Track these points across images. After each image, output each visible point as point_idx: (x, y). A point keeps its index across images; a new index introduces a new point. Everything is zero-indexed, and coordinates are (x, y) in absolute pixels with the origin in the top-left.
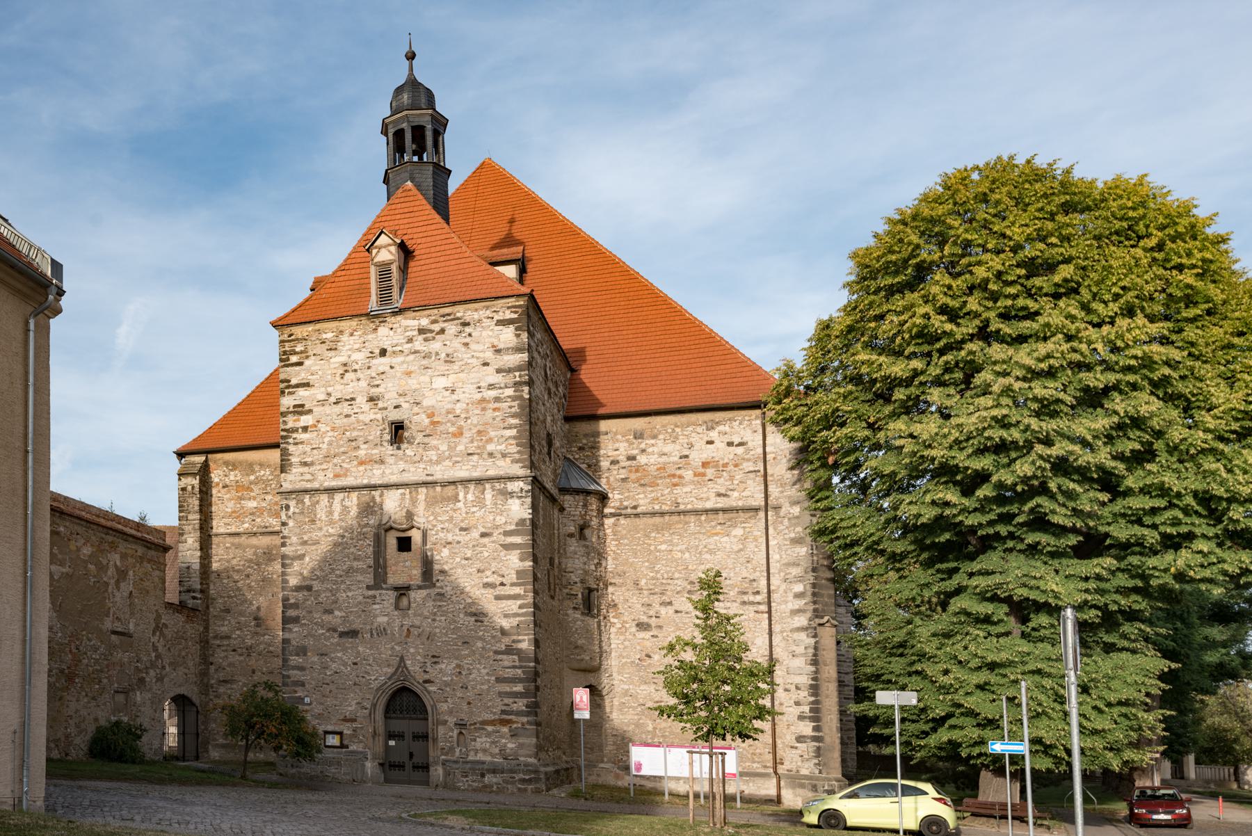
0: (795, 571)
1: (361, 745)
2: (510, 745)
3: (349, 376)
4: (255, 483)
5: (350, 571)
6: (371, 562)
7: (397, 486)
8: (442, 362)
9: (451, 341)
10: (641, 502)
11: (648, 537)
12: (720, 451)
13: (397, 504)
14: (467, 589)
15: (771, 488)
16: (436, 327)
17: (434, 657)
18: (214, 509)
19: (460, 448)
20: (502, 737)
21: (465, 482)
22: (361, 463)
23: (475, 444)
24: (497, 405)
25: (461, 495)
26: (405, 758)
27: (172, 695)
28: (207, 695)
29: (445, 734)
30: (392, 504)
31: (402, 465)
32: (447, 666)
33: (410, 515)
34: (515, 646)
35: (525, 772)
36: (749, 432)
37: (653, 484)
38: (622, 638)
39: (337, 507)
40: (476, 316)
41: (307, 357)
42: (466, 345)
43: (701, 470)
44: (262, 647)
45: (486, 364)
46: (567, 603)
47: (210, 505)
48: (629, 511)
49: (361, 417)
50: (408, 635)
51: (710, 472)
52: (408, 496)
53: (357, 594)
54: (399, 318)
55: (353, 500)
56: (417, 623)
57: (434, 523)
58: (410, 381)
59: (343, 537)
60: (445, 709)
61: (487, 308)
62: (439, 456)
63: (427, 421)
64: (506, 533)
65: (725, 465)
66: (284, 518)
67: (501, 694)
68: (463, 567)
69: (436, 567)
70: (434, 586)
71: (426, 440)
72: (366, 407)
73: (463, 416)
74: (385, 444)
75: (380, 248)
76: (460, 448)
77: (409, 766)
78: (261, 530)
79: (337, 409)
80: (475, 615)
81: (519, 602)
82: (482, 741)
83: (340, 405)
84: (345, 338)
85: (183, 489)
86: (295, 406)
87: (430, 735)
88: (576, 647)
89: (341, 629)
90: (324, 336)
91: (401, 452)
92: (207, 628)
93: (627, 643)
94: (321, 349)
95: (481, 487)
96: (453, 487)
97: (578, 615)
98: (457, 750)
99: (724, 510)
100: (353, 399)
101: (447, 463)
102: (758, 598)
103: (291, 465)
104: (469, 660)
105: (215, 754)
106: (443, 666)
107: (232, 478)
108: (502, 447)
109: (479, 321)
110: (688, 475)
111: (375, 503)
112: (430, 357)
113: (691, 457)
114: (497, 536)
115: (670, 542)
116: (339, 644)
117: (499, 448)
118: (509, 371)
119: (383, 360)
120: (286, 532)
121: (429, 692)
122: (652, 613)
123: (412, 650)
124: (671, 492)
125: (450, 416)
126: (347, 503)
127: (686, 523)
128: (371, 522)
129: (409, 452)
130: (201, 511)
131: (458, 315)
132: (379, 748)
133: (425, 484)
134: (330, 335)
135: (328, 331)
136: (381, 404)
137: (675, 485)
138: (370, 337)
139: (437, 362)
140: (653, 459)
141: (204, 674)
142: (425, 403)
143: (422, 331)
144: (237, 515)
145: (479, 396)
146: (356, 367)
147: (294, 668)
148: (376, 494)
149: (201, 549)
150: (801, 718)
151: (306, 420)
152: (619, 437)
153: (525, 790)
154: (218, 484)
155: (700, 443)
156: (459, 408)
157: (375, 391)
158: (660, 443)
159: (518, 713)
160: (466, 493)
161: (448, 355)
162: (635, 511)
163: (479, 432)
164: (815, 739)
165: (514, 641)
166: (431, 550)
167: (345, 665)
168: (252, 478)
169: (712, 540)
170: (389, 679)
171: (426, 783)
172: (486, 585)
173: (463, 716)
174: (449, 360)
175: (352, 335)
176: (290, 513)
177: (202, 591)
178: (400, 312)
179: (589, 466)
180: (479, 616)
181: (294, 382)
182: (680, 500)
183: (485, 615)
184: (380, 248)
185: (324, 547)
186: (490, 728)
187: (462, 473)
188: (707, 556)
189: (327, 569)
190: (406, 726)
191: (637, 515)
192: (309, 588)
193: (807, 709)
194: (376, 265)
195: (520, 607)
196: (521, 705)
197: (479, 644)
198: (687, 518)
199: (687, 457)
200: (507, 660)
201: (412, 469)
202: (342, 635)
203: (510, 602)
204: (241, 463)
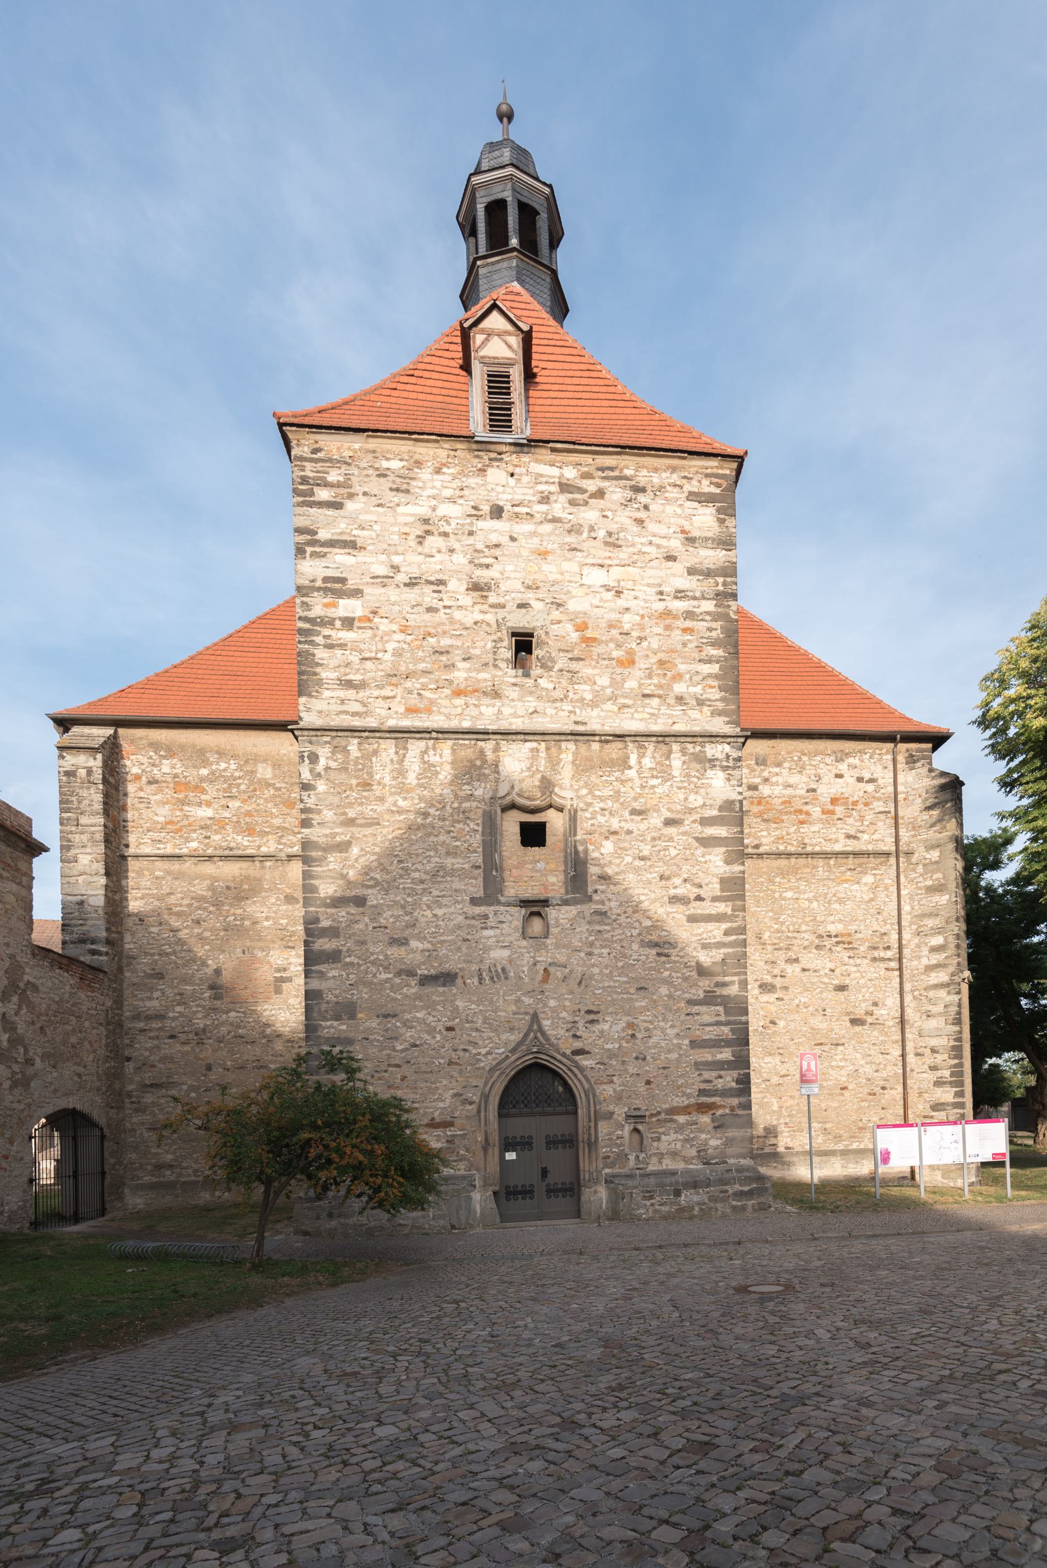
1: (462, 1165)
2: (714, 1143)
3: (433, 542)
4: (213, 778)
5: (437, 874)
7: (526, 735)
8: (598, 543)
9: (611, 510)
10: (764, 841)
11: (771, 881)
12: (848, 786)
13: (523, 766)
14: (645, 905)
15: (902, 832)
16: (591, 486)
17: (589, 1012)
18: (130, 816)
19: (631, 684)
20: (702, 1131)
21: (640, 737)
22: (458, 693)
23: (655, 681)
24: (688, 624)
25: (633, 759)
27: (50, 1110)
28: (120, 1108)
29: (612, 1134)
30: (516, 764)
31: (532, 703)
32: (612, 1027)
33: (547, 785)
34: (719, 991)
36: (880, 767)
37: (778, 821)
40: (656, 480)
41: (351, 496)
42: (640, 522)
44: (224, 1029)
45: (671, 558)
47: (124, 808)
49: (458, 615)
51: (839, 810)
52: (543, 755)
54: (525, 458)
55: (444, 753)
56: (562, 959)
57: (589, 799)
58: (545, 567)
59: (426, 815)
60: (609, 1094)
61: (674, 469)
62: (596, 694)
64: (705, 822)
66: (306, 775)
67: (698, 1066)
68: (637, 871)
69: (593, 870)
70: (590, 899)
71: (574, 666)
72: (467, 600)
73: (635, 634)
74: (503, 665)
75: (489, 334)
76: (631, 684)
78: (219, 852)
79: (412, 595)
80: (657, 945)
81: (725, 926)
82: (670, 1140)
83: (416, 590)
84: (425, 474)
85: (68, 774)
86: (325, 579)
87: (582, 1135)
89: (422, 971)
90: (385, 464)
91: (529, 682)
92: (119, 1003)
94: (375, 485)
96: (619, 745)
98: (632, 1157)
99: (856, 854)
100: (441, 582)
101: (609, 706)
102: (889, 954)
103: (320, 683)
104: (648, 1016)
105: (136, 1201)
106: (606, 1027)
107: (166, 769)
108: (698, 689)
109: (661, 488)
110: (816, 811)
111: (485, 761)
112: (579, 532)
113: (819, 791)
114: (689, 824)
117: (692, 689)
118: (708, 573)
119: (496, 524)
120: (311, 802)
121: (582, 1069)
122: (776, 971)
123: (552, 1003)
124: (798, 831)
125: (614, 632)
126: (432, 758)
127: (814, 867)
128: (479, 793)
129: (543, 683)
130: (106, 813)
131: (628, 472)
132: (494, 1167)
134: (395, 464)
135: (395, 454)
136: (493, 599)
137: (802, 822)
138: (473, 481)
139: (592, 543)
140: (777, 790)
141: (115, 1075)
142: (573, 605)
143: (565, 487)
144: (177, 828)
145: (660, 606)
146: (447, 529)
148: (488, 746)
149: (107, 874)
151: (347, 607)
153: (743, 1208)
154: (138, 777)
155: (828, 778)
156: (628, 621)
157: (482, 575)
158: (785, 772)
159: (725, 1093)
160: (641, 756)
161: (610, 534)
163: (661, 663)
165: (717, 985)
166: (584, 842)
167: (431, 1031)
168: (204, 772)
169: (840, 888)
170: (513, 1051)
172: (674, 900)
173: (638, 1103)
174: (613, 542)
175: (438, 471)
176: (320, 768)
177: (108, 942)
178: (531, 444)
180: (663, 946)
181: (323, 535)
182: (807, 841)
183: (673, 945)
184: (489, 334)
185: (389, 831)
186: (681, 1119)
188: (836, 906)
189: (395, 868)
190: (536, 1126)
191: (760, 856)
192: (360, 901)
193: (947, 1073)
195: (726, 933)
196: (728, 1079)
197: (664, 990)
198: (815, 862)
199: (814, 790)
200: (708, 1014)
201: (550, 711)
203: (711, 926)
204: (182, 747)
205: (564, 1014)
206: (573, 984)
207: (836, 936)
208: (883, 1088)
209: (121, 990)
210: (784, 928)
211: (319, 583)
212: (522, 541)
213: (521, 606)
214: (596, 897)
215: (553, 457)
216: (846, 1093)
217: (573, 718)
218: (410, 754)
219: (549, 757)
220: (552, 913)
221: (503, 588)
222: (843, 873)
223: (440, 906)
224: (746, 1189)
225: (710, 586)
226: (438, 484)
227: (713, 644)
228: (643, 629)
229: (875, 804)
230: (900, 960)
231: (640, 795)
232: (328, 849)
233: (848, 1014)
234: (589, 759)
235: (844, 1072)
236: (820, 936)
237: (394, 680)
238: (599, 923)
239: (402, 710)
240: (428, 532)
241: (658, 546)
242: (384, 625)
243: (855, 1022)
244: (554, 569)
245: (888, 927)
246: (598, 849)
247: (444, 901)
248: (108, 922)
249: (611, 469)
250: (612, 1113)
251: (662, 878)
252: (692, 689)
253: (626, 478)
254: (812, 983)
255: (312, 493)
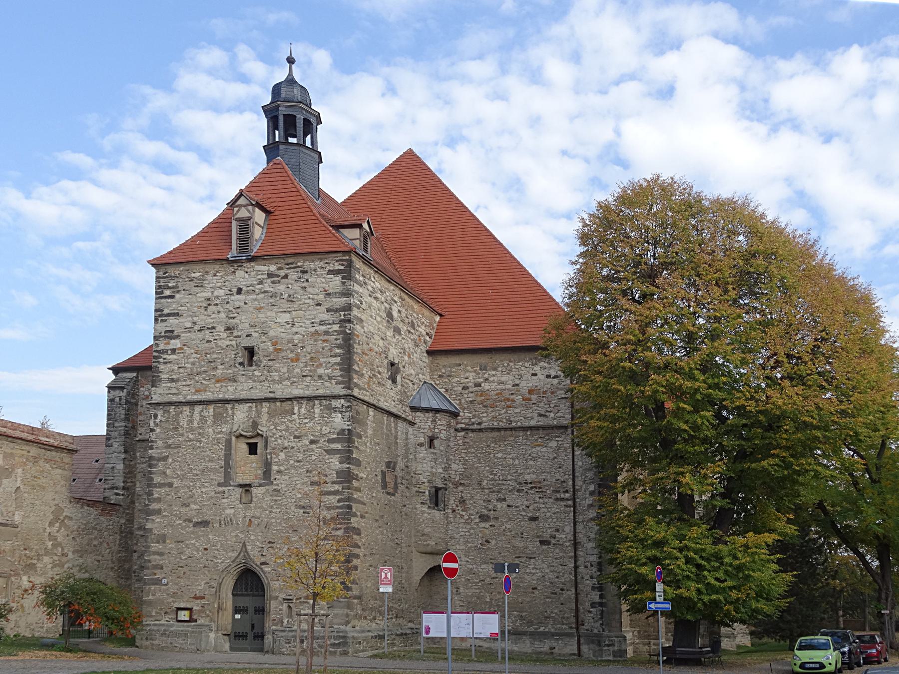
0: (590, 475)
6: (222, 463)
10: (484, 419)
16: (282, 273)
17: (270, 542)
19: (297, 370)
21: (299, 399)
22: (218, 381)
24: (326, 337)
25: (296, 409)
26: (248, 629)
31: (251, 383)
33: (255, 425)
35: (335, 638)
38: (468, 527)
39: (196, 417)
41: (178, 292)
43: (528, 396)
46: (415, 499)
48: (475, 426)
49: (219, 343)
50: (249, 525)
51: (534, 397)
53: (210, 490)
54: (253, 264)
56: (258, 514)
57: (274, 431)
61: (321, 260)
63: (271, 349)
64: (330, 441)
65: (545, 392)
68: (295, 468)
71: (271, 363)
76: (297, 370)
77: (250, 636)
79: (200, 335)
81: (338, 497)
86: (166, 332)
88: (424, 535)
90: (193, 275)
92: (131, 521)
93: (472, 531)
95: (311, 403)
96: (290, 403)
97: (425, 508)
99: (544, 428)
100: (214, 328)
102: (567, 495)
112: (276, 297)
115: (504, 452)
116: (193, 533)
117: (326, 371)
118: (337, 311)
119: (239, 296)
122: (490, 507)
123: (252, 537)
126: (205, 413)
133: (267, 400)
138: (229, 278)
140: (493, 386)
142: (272, 333)
143: (270, 275)
147: (155, 553)
150: (593, 588)
151: (175, 343)
152: (469, 368)
153: (335, 653)
160: (301, 407)
161: (290, 296)
162: (479, 427)
164: (601, 604)
167: (198, 550)
171: (261, 650)
175: (215, 275)
176: (158, 421)
179: (447, 390)
181: (166, 311)
182: (512, 419)
184: (240, 206)
187: (297, 392)
188: (531, 463)
194: (237, 220)
195: (339, 501)
199: (517, 385)
202: (196, 524)
203: (331, 497)
205: (258, 543)
206: (262, 527)
207: (531, 483)
208: (562, 590)
209: (133, 513)
210: (496, 478)
211: (163, 334)
212: (250, 304)
213: (247, 336)
214: (275, 482)
215: (263, 262)
216: (537, 592)
217: (269, 390)
218: (196, 412)
219: (257, 411)
220: (254, 490)
221: (240, 327)
222: (536, 440)
223: (205, 487)
224: (337, 642)
225: (336, 317)
226: (215, 281)
227: (338, 347)
228: (303, 343)
229: (559, 392)
230: (574, 500)
231: (299, 428)
232: (159, 460)
233: (538, 537)
234: (275, 410)
235: (534, 577)
236: (520, 483)
237: (191, 377)
238: (277, 496)
239: (193, 391)
240: (209, 305)
241: (313, 299)
242: (188, 351)
243: (542, 542)
244: (263, 316)
245: (567, 476)
246: (277, 457)
247: (206, 485)
248: (125, 477)
249: (291, 264)
250: (277, 597)
251: (307, 471)
252: (326, 371)
253: (299, 267)
254: (514, 515)
255: (162, 293)
